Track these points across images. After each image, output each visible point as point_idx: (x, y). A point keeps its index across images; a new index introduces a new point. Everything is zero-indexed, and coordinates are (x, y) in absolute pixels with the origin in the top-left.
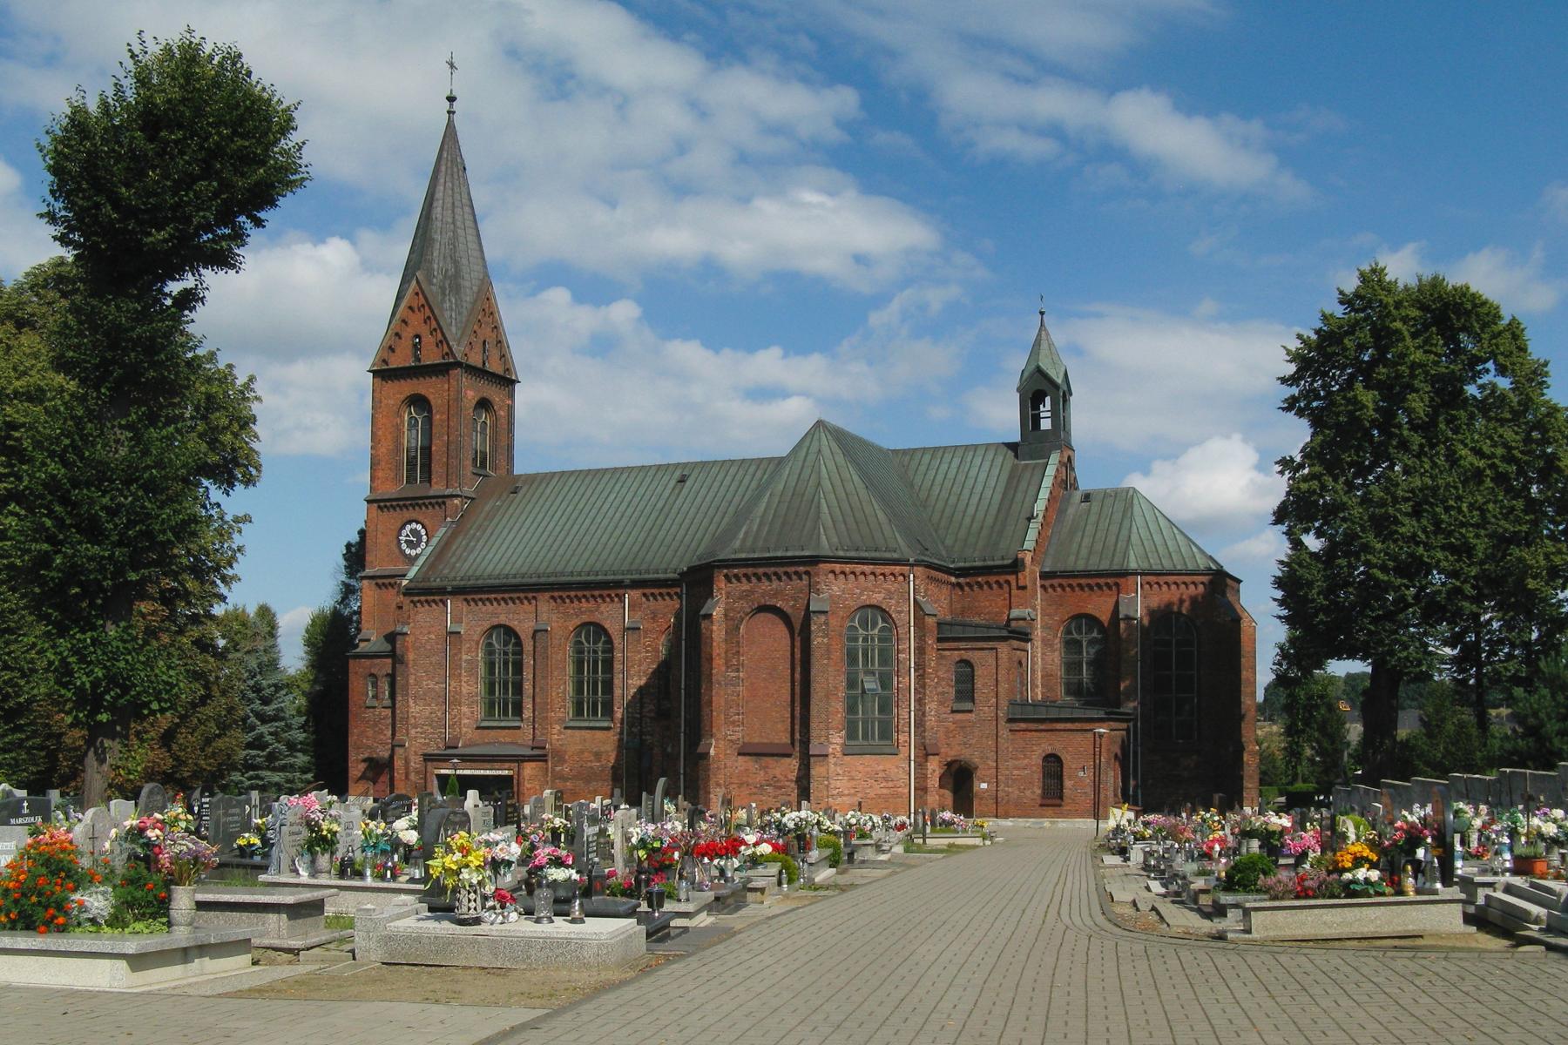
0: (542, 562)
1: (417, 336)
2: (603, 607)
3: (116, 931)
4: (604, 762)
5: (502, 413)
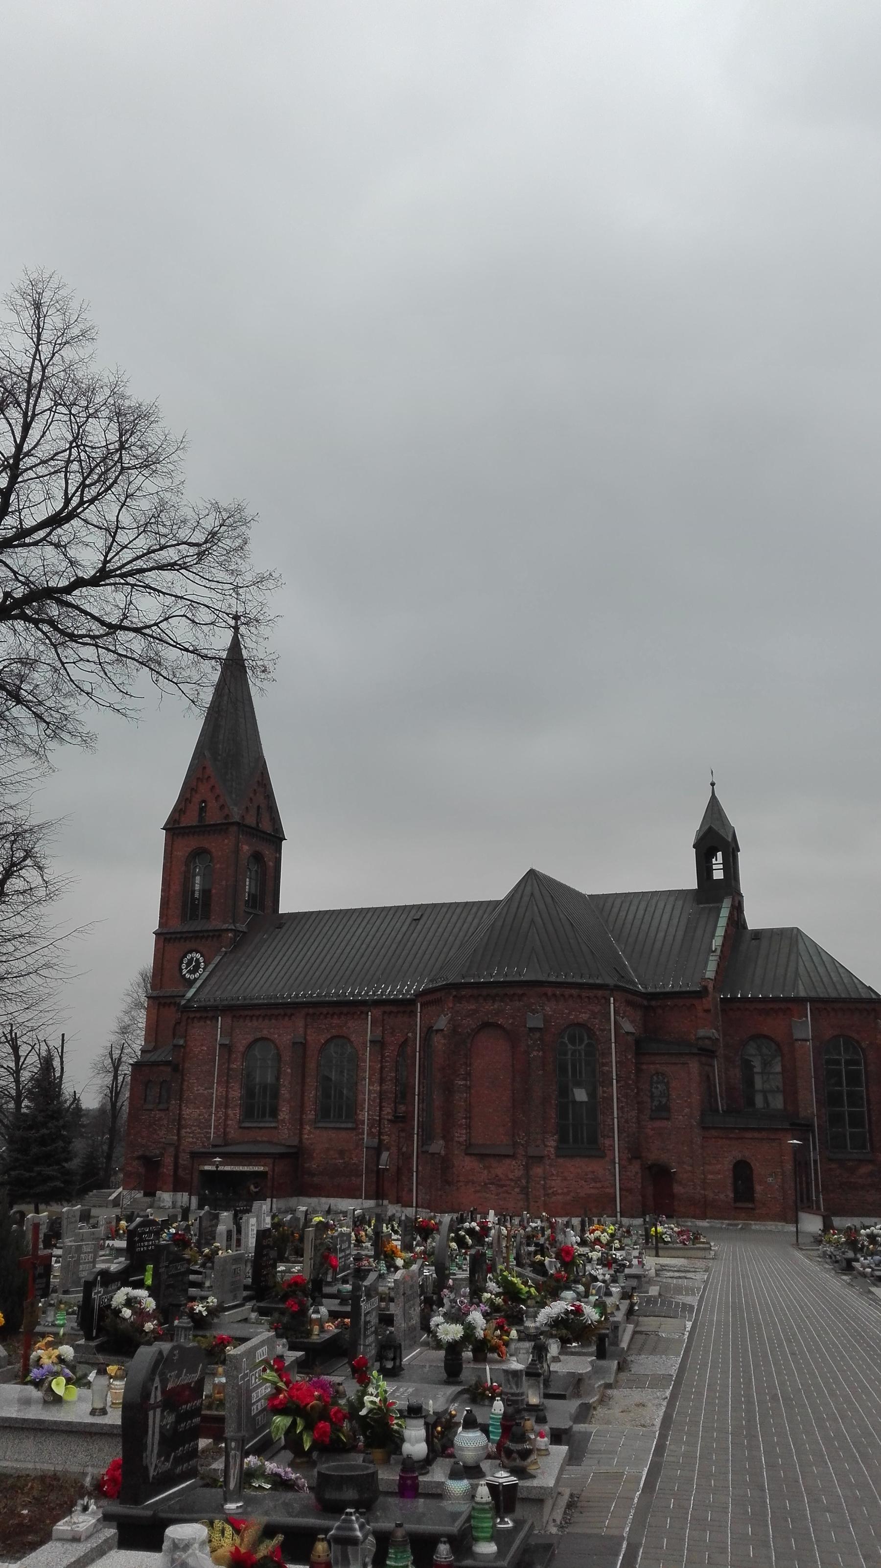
1: (204, 801)
4: (347, 1159)
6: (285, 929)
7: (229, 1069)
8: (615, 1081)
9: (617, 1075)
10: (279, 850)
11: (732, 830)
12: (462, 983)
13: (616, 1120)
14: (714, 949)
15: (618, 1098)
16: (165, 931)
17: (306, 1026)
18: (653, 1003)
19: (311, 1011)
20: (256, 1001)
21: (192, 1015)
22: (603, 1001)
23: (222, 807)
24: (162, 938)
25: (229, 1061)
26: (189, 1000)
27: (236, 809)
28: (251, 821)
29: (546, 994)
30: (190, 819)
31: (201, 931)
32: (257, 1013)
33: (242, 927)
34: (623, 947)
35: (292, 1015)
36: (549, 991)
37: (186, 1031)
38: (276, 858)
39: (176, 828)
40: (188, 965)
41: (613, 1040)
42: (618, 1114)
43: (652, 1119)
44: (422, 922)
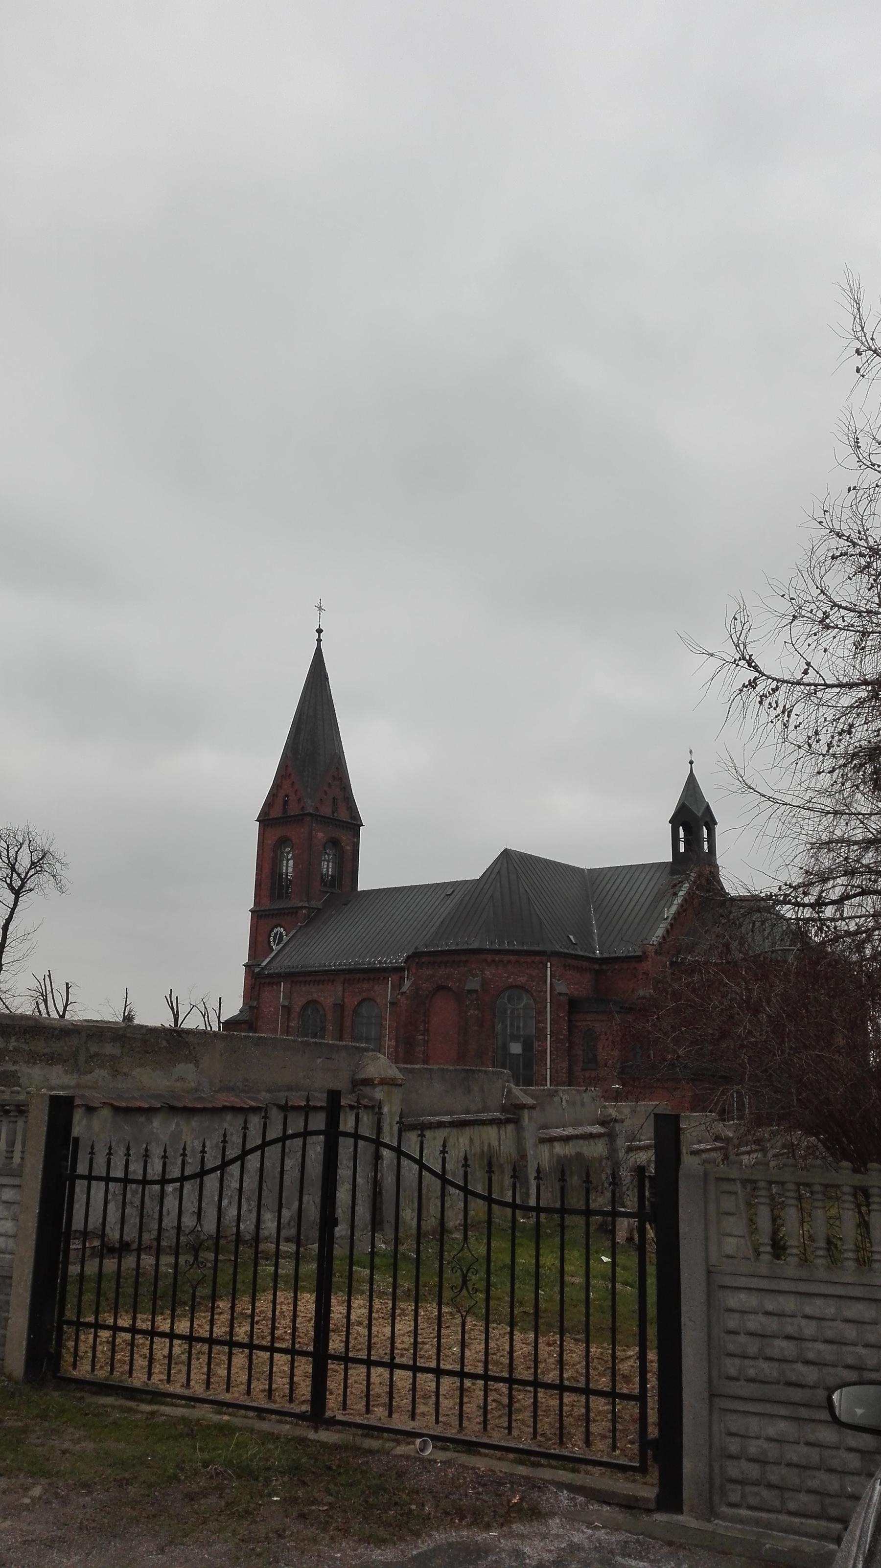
0: (610, 911)
1: (287, 796)
2: (376, 988)
3: (587, 1097)
5: (348, 848)
6: (349, 906)
7: (288, 1026)
8: (549, 1036)
9: (551, 1031)
10: (357, 835)
11: (705, 805)
12: (424, 952)
13: (548, 1070)
14: (665, 917)
15: (551, 1051)
16: (258, 909)
17: (344, 990)
18: (604, 967)
19: (347, 976)
20: (313, 969)
21: (263, 981)
22: (541, 966)
23: (299, 800)
24: (256, 914)
25: (288, 1020)
26: (263, 968)
27: (309, 802)
28: (326, 811)
29: (486, 960)
30: (276, 813)
31: (283, 909)
32: (309, 979)
33: (315, 904)
34: (598, 916)
35: (334, 980)
36: (489, 958)
37: (259, 995)
38: (354, 842)
39: (267, 820)
40: (275, 937)
41: (549, 1000)
42: (550, 1065)
43: (583, 1070)
44: (452, 897)
